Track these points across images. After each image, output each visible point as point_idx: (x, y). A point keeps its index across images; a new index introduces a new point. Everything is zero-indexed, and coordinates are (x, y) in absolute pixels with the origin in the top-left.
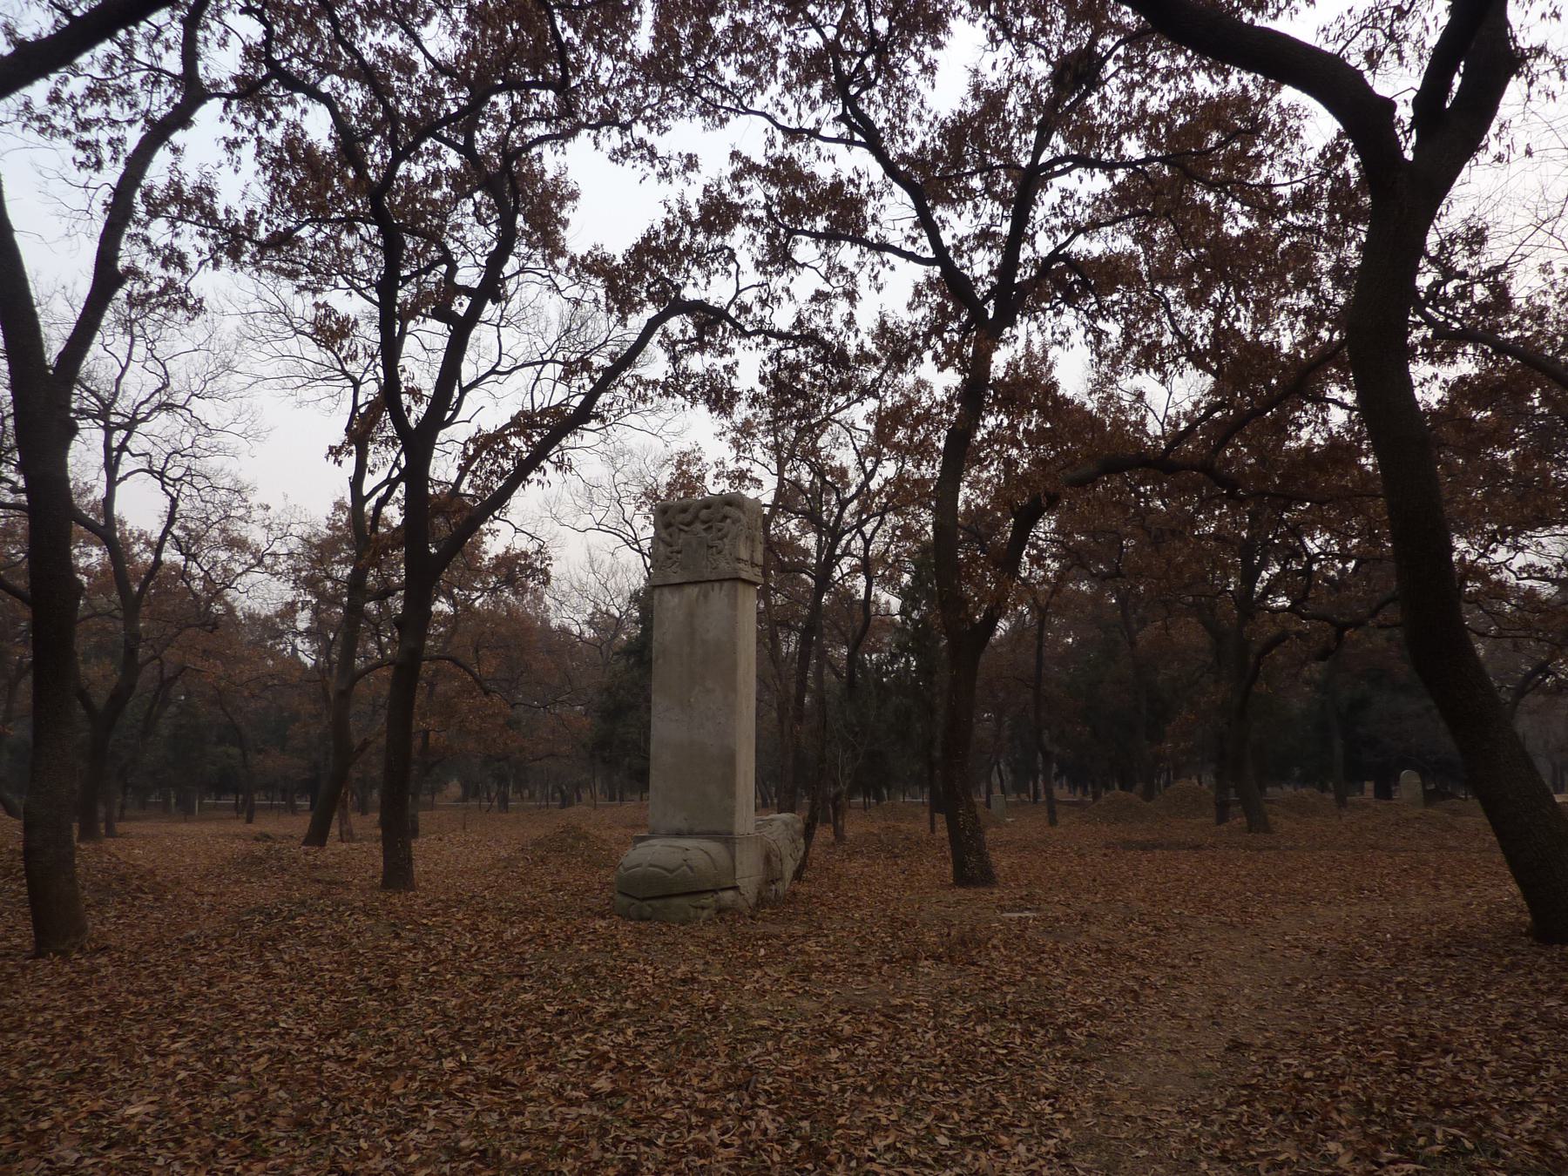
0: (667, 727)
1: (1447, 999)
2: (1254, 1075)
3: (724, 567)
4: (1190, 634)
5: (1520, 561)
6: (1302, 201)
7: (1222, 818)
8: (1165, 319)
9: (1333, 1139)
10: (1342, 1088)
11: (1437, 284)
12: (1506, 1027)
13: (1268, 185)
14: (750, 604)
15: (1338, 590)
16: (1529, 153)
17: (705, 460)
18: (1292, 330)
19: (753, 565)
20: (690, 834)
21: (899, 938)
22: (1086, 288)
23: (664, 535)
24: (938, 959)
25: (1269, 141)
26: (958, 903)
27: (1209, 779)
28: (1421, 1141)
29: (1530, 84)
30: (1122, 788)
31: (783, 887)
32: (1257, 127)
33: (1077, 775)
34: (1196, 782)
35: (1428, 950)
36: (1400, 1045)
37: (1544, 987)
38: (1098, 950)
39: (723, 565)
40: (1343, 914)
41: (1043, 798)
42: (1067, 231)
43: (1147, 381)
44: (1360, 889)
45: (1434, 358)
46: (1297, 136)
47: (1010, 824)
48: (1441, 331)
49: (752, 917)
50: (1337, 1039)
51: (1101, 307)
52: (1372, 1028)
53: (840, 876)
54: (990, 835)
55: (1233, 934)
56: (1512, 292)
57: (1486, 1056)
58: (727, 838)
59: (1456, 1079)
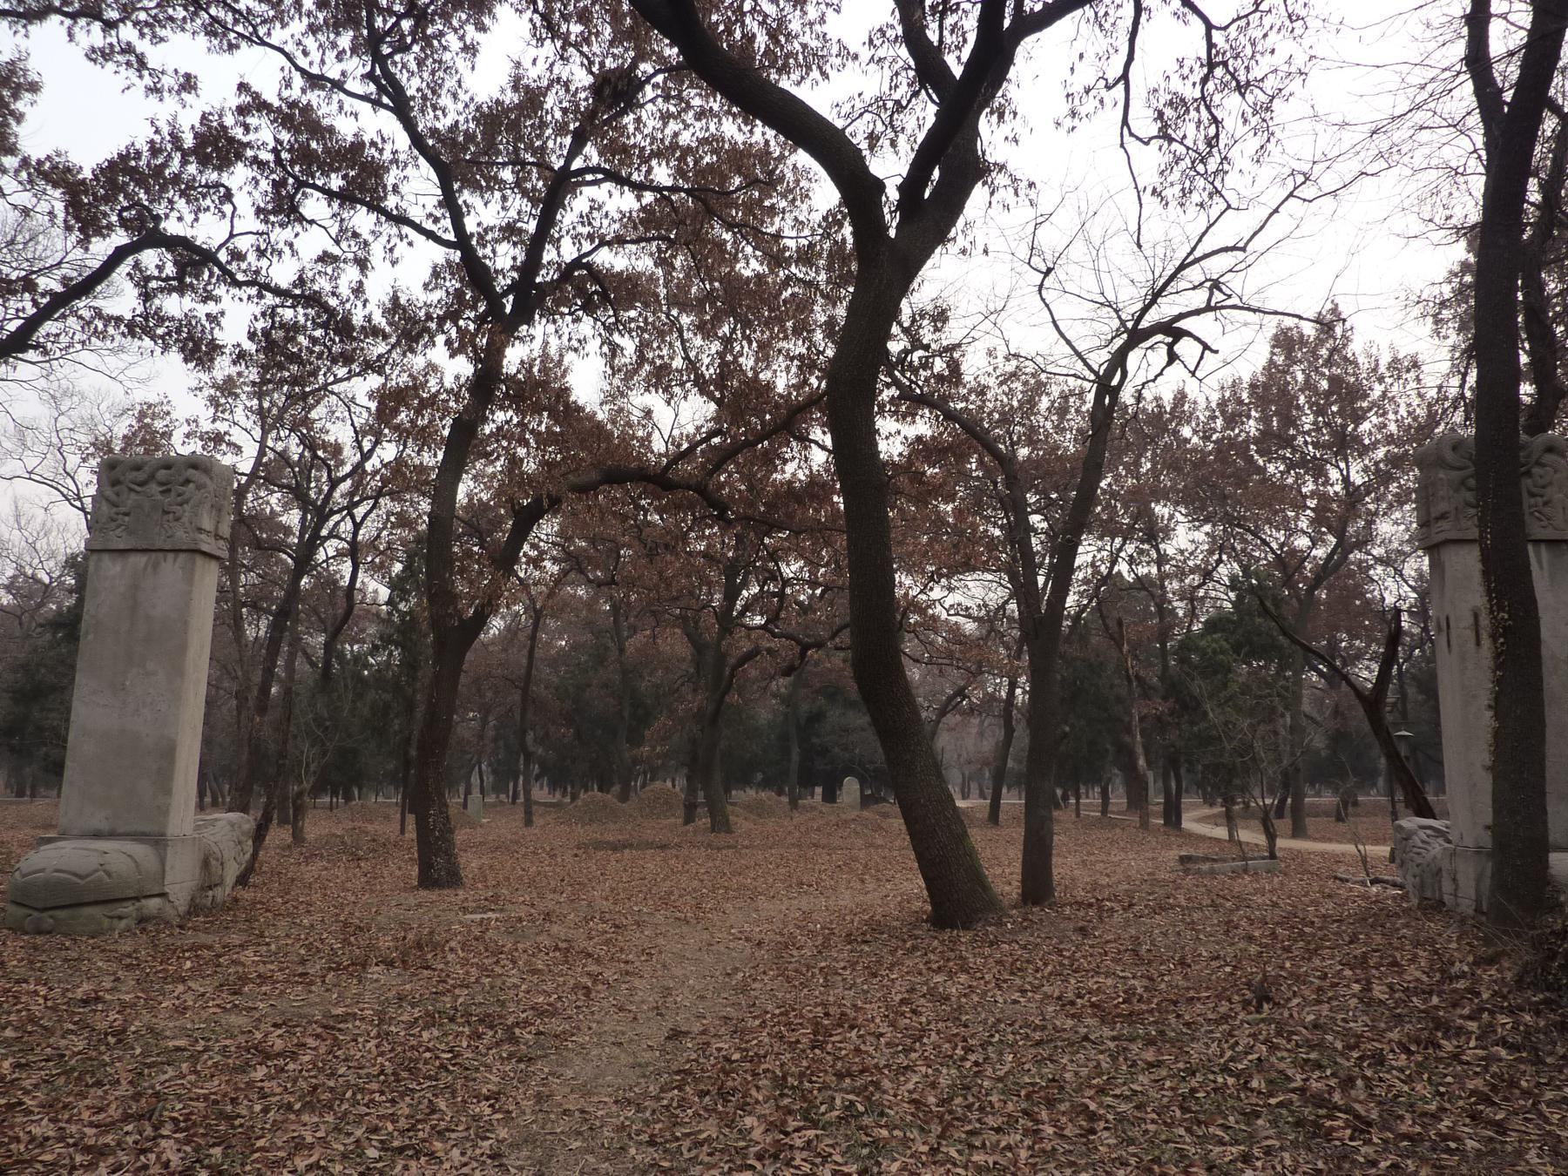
0: (91, 713)
2: (688, 1061)
3: (182, 536)
4: (674, 644)
6: (806, 256)
7: (689, 819)
8: (678, 344)
9: (750, 1114)
11: (906, 352)
12: (902, 1002)
13: (778, 236)
14: (209, 579)
15: (805, 613)
16: (986, 252)
17: (174, 416)
19: (218, 537)
20: (112, 835)
21: (350, 944)
23: (109, 492)
24: (390, 964)
25: (784, 196)
26: (419, 905)
27: (681, 782)
28: (823, 1109)
29: (992, 194)
30: (600, 790)
31: (221, 894)
32: (771, 183)
33: (558, 777)
34: (669, 784)
35: (849, 938)
37: (935, 966)
38: (557, 948)
39: (180, 533)
41: (521, 800)
42: (592, 242)
43: (655, 400)
45: (902, 417)
47: (483, 824)
48: (906, 394)
49: (181, 927)
53: (293, 880)
54: (460, 837)
55: (685, 929)
56: (963, 368)
58: (157, 840)
59: (857, 1050)
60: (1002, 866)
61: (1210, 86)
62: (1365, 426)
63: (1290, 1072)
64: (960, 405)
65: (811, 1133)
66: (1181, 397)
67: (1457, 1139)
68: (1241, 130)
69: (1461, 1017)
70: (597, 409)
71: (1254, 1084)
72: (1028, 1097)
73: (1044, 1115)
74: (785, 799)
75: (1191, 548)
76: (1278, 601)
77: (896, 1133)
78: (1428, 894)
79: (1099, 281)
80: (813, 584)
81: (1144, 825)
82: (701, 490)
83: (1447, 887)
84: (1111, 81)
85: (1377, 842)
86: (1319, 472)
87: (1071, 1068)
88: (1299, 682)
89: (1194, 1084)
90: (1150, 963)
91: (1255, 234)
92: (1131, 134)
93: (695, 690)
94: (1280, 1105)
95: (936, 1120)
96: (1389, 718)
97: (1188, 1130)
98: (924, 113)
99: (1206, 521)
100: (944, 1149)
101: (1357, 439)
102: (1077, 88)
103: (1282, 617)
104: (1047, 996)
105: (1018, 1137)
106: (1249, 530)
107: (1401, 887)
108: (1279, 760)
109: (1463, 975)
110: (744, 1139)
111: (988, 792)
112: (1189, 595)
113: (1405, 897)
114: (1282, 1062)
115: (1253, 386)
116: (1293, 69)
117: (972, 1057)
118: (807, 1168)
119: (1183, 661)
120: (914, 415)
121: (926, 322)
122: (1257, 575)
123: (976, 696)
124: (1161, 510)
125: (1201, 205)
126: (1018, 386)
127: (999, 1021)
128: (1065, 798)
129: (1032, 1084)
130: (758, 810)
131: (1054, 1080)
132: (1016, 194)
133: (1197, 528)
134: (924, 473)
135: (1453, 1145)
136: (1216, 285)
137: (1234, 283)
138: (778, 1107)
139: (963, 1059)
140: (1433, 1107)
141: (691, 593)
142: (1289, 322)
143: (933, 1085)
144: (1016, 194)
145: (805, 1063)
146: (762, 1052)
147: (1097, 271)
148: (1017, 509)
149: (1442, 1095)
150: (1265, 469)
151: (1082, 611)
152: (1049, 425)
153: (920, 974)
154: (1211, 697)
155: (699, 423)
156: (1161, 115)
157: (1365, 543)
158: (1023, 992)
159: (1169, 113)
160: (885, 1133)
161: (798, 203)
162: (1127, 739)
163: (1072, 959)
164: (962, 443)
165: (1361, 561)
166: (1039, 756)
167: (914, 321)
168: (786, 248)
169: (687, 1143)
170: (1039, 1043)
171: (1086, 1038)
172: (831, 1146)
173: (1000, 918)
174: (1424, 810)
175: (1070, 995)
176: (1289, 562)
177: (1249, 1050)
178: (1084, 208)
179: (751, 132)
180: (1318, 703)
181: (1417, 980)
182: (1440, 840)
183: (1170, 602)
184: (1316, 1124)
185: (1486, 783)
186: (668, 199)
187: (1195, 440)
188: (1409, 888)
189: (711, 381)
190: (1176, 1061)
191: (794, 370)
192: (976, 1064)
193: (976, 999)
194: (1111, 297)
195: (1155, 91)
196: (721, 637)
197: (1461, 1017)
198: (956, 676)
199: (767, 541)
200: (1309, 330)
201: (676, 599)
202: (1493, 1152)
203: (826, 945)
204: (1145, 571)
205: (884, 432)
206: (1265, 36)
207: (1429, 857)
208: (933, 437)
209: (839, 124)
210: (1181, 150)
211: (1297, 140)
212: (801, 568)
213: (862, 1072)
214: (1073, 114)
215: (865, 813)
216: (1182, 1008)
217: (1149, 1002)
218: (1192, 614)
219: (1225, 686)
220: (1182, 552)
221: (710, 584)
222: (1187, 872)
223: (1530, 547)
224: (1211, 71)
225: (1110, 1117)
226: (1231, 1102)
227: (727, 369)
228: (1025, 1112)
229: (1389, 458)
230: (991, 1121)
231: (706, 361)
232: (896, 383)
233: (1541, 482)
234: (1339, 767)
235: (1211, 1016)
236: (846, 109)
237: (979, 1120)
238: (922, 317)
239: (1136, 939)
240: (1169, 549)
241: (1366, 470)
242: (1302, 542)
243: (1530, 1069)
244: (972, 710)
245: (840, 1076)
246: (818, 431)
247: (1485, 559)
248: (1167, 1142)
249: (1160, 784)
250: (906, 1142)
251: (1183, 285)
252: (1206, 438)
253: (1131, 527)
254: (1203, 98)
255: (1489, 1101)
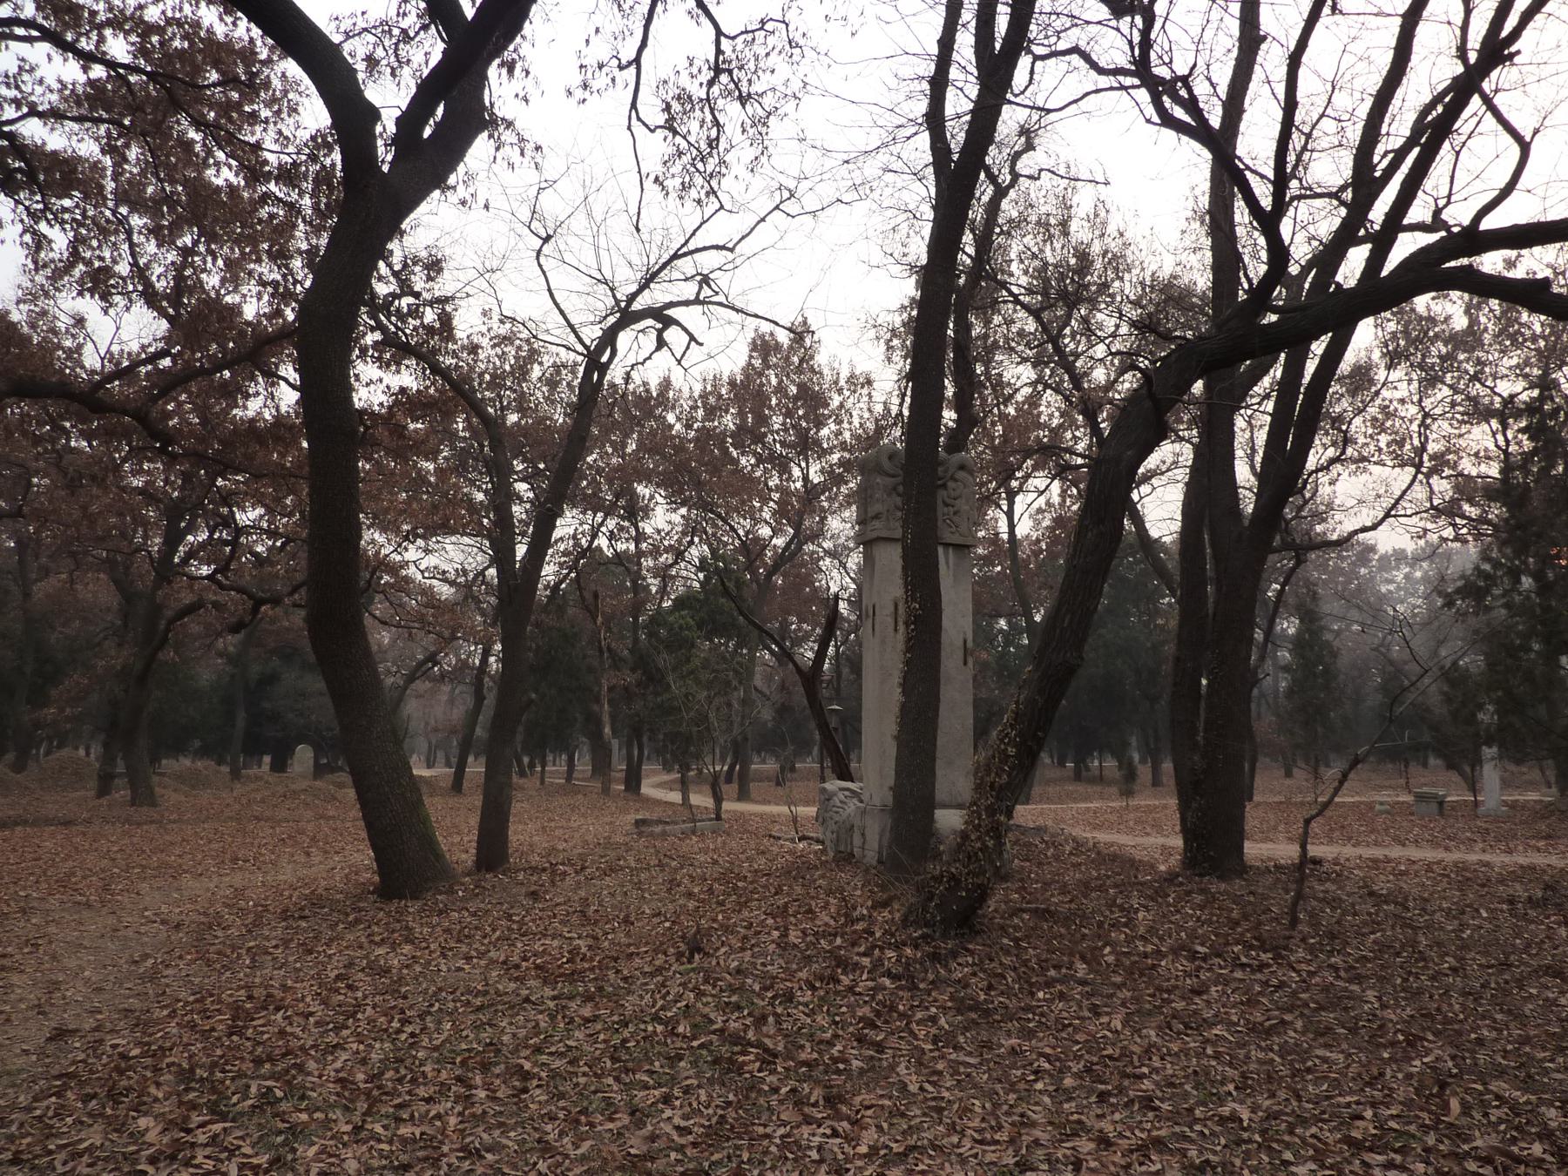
1: (291, 959)
2: (74, 1062)
4: (98, 591)
5: (431, 561)
6: (288, 175)
7: (104, 789)
8: (126, 246)
9: (146, 1114)
10: (168, 1060)
11: (394, 296)
12: (338, 978)
13: (257, 147)
15: (261, 565)
16: (487, 207)
18: (259, 299)
22: (31, 181)
25: (268, 105)
27: (96, 750)
28: (235, 1099)
29: (497, 149)
32: (252, 87)
34: (82, 752)
35: (285, 915)
36: (236, 1009)
37: (377, 939)
40: (212, 885)
42: (18, 108)
43: (89, 306)
44: (235, 860)
45: (384, 365)
46: (295, 111)
48: (389, 341)
50: (174, 1011)
51: (47, 208)
52: (212, 995)
55: (86, 914)
56: (455, 322)
57: (315, 1007)
59: (282, 1033)
60: (455, 830)
61: (715, 90)
62: (825, 432)
63: (712, 1016)
64: (449, 361)
65: (217, 1127)
66: (666, 384)
67: (845, 1061)
68: (738, 137)
69: (858, 954)
70: (12, 307)
71: (681, 1029)
72: (463, 1063)
73: (478, 1080)
74: (225, 769)
75: (667, 528)
76: (740, 583)
77: (316, 1116)
78: (842, 848)
79: (598, 256)
80: (272, 534)
81: (606, 791)
82: (141, 417)
83: (857, 841)
84: (624, 62)
85: (807, 803)
86: (784, 469)
87: (509, 1030)
88: (752, 658)
89: (626, 1034)
90: (596, 922)
91: (743, 238)
92: (639, 119)
93: (120, 645)
94: (701, 1046)
95: (363, 1097)
96: (825, 693)
97: (617, 1079)
98: (430, 50)
99: (683, 504)
100: (369, 1127)
101: (818, 443)
102: (591, 61)
103: (743, 597)
104: (492, 961)
105: (449, 1105)
106: (719, 516)
107: (822, 843)
108: (729, 730)
109: (862, 918)
110: (134, 1143)
111: (454, 760)
112: (663, 574)
113: (823, 852)
114: (707, 1007)
115: (732, 383)
116: (789, 92)
117: (409, 1029)
118: (209, 1165)
119: (650, 635)
120: (398, 364)
121: (417, 269)
122: (723, 558)
123: (449, 661)
124: (642, 490)
125: (699, 202)
126: (511, 351)
127: (440, 989)
128: (532, 765)
129: (468, 1050)
130: (193, 781)
131: (491, 1044)
132: (522, 154)
133: (675, 510)
134: (405, 427)
135: (841, 1066)
136: (705, 280)
137: (721, 280)
138: (181, 1103)
139: (399, 1031)
140: (828, 1035)
141: (123, 535)
142: (766, 327)
143: (364, 1062)
144: (522, 154)
145: (219, 1052)
146: (168, 1044)
147: (597, 248)
148: (500, 473)
149: (836, 1023)
150: (737, 462)
151: (561, 582)
152: (539, 395)
153: (361, 947)
154: (674, 670)
155: (146, 342)
156: (668, 108)
157: (817, 536)
158: (468, 959)
159: (676, 107)
160: (304, 1117)
161: (284, 115)
162: (596, 708)
163: (521, 923)
164: (451, 399)
165: (814, 552)
166: (503, 724)
167: (405, 266)
168: (266, 162)
169: (62, 1156)
170: (479, 1009)
171: (527, 1000)
172: (242, 1138)
173: (451, 887)
174: (845, 775)
175: (516, 959)
176: (752, 548)
177: (679, 997)
178: (588, 183)
179: (234, 24)
180: (769, 679)
181: (826, 924)
182: (855, 801)
183: (644, 579)
184: (731, 1061)
185: (892, 749)
186: (124, 79)
187: (678, 427)
188: (828, 843)
189: (166, 297)
190: (612, 1014)
191: (266, 298)
192: (412, 1035)
193: (418, 969)
194: (608, 276)
195: (665, 82)
196: (157, 585)
197: (858, 954)
198: (429, 641)
199: (220, 482)
200: (783, 337)
201: (102, 539)
202: (872, 1068)
203: (257, 923)
204: (624, 547)
205: (364, 378)
206: (767, 54)
207: (845, 815)
208: (418, 391)
209: (336, 38)
210: (684, 145)
211: (786, 159)
212: (261, 517)
213: (284, 1055)
214: (585, 86)
215: (318, 783)
216: (622, 964)
217: (592, 960)
218: (663, 591)
219: (688, 660)
220: (659, 532)
221: (145, 523)
222: (640, 834)
223: (940, 550)
224: (716, 76)
225: (543, 1074)
226: (658, 1048)
227: (182, 286)
228: (459, 1079)
229: (841, 463)
230: (422, 1092)
231: (158, 270)
232: (380, 327)
233: (953, 494)
234: (781, 739)
235: (647, 969)
236: (346, 25)
237: (409, 1093)
238: (415, 264)
239: (585, 902)
240: (647, 527)
241: (822, 471)
242: (765, 531)
243: (906, 994)
244: (443, 676)
245: (258, 1062)
246: (290, 369)
247: (905, 557)
248: (595, 1092)
249: (624, 751)
250: (327, 1124)
251: (676, 275)
252: (688, 427)
253: (614, 504)
254: (708, 100)
255: (874, 1026)
